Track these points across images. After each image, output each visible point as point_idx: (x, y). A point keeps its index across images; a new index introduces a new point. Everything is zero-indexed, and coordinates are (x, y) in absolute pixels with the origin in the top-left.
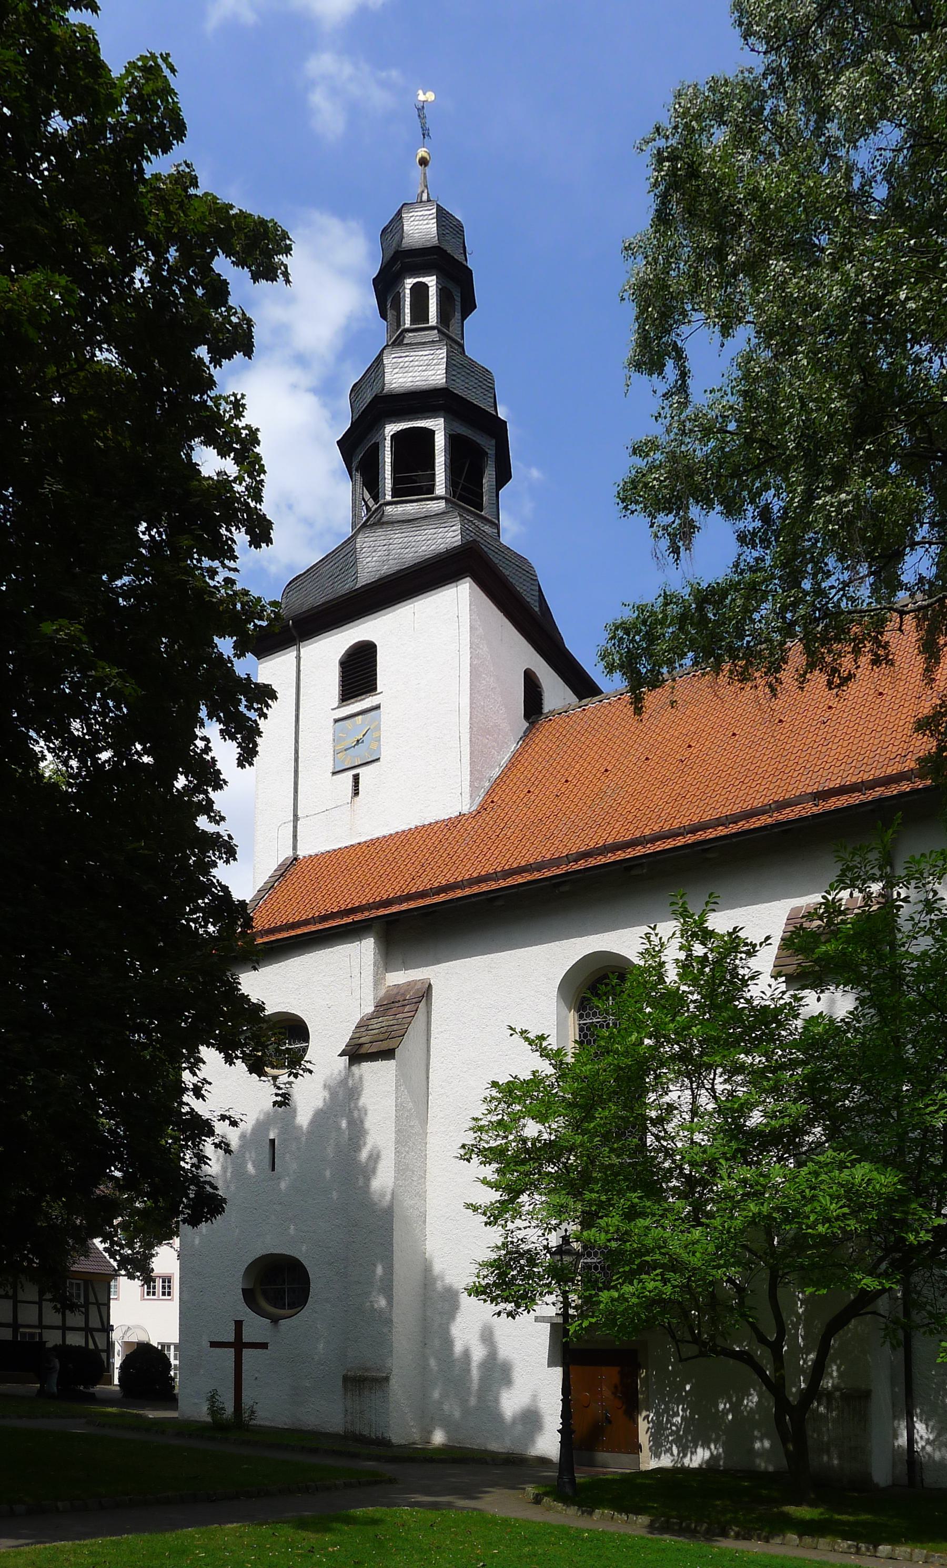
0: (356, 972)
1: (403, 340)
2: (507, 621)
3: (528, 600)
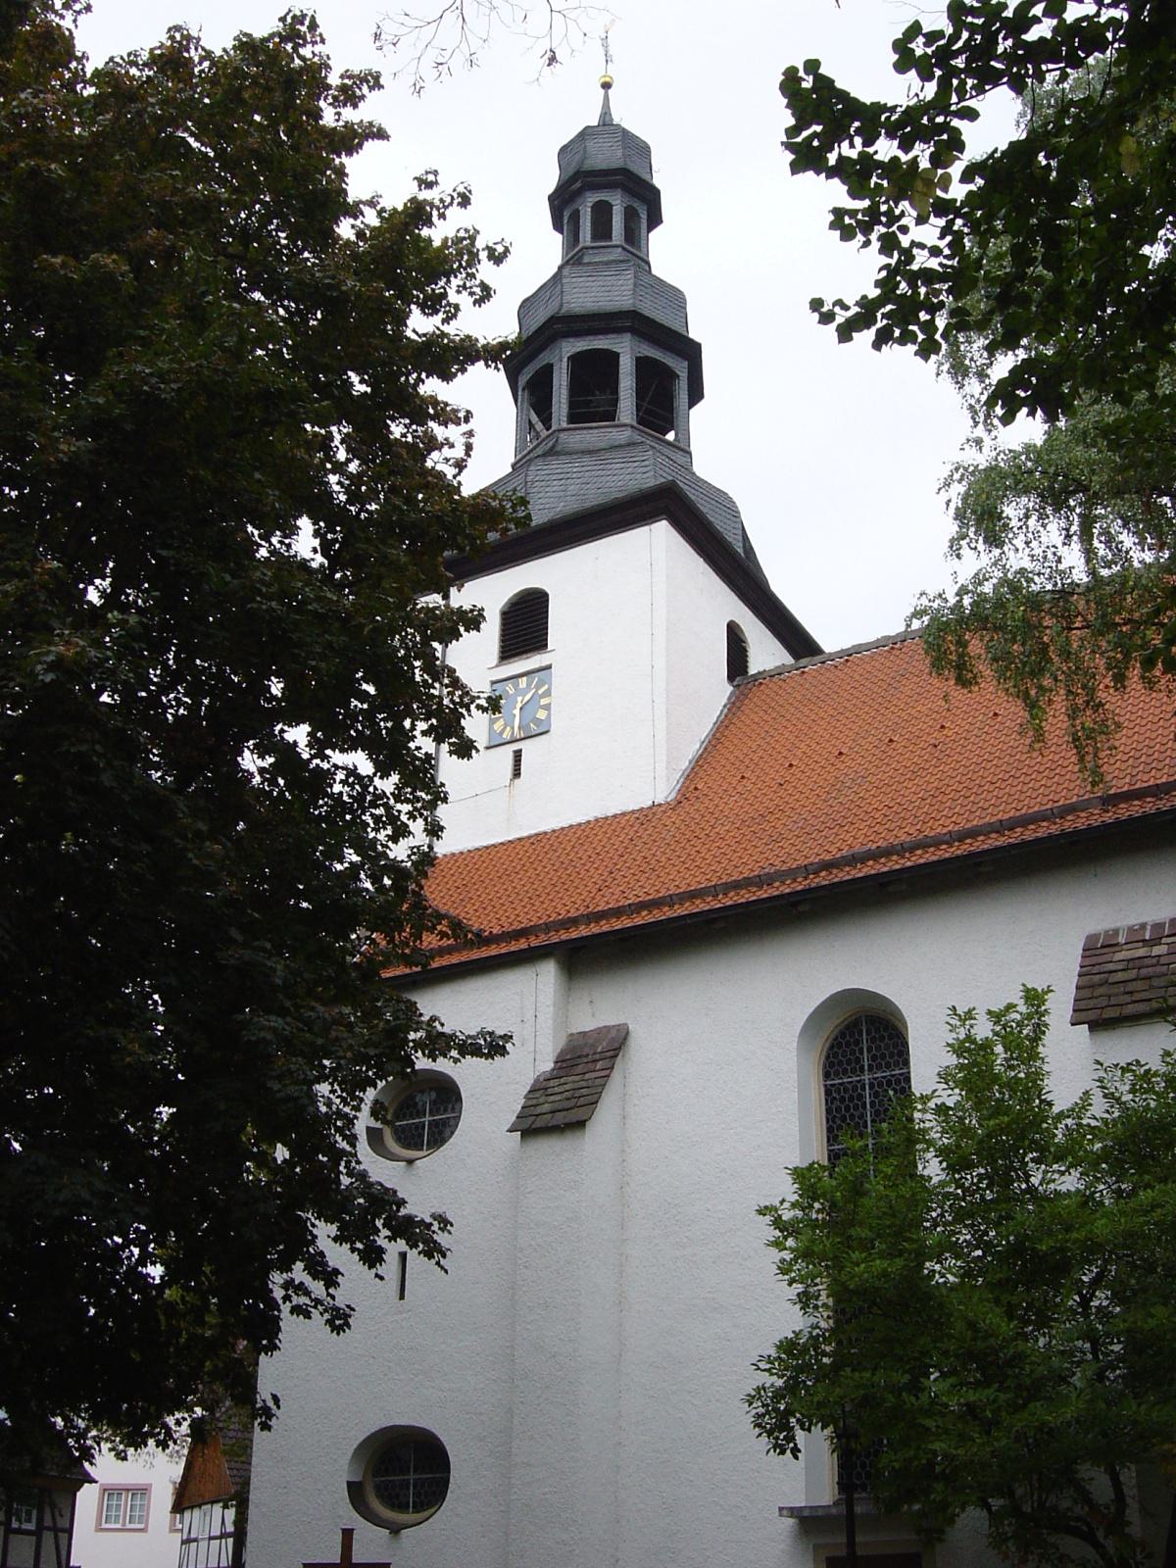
0: (529, 1015)
1: (581, 258)
2: (707, 566)
3: (730, 540)
